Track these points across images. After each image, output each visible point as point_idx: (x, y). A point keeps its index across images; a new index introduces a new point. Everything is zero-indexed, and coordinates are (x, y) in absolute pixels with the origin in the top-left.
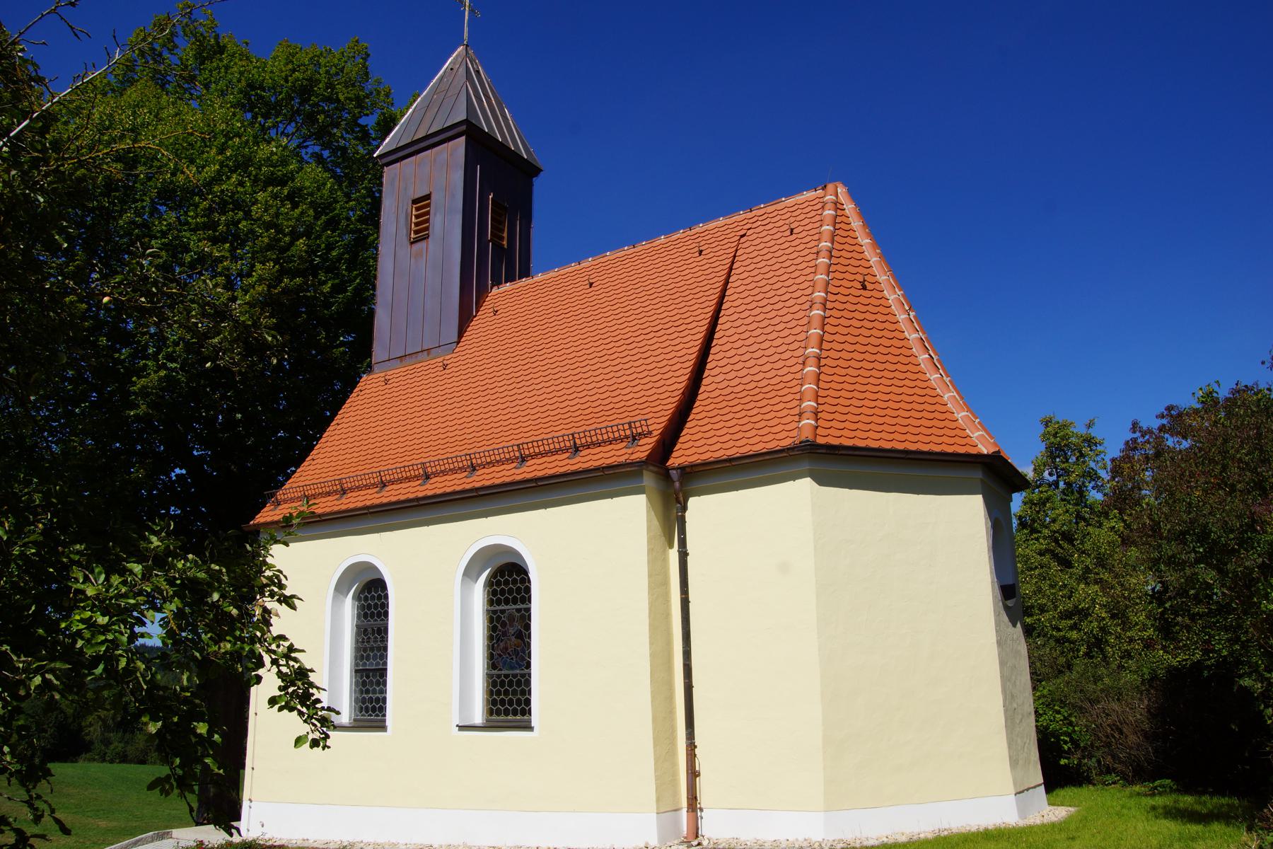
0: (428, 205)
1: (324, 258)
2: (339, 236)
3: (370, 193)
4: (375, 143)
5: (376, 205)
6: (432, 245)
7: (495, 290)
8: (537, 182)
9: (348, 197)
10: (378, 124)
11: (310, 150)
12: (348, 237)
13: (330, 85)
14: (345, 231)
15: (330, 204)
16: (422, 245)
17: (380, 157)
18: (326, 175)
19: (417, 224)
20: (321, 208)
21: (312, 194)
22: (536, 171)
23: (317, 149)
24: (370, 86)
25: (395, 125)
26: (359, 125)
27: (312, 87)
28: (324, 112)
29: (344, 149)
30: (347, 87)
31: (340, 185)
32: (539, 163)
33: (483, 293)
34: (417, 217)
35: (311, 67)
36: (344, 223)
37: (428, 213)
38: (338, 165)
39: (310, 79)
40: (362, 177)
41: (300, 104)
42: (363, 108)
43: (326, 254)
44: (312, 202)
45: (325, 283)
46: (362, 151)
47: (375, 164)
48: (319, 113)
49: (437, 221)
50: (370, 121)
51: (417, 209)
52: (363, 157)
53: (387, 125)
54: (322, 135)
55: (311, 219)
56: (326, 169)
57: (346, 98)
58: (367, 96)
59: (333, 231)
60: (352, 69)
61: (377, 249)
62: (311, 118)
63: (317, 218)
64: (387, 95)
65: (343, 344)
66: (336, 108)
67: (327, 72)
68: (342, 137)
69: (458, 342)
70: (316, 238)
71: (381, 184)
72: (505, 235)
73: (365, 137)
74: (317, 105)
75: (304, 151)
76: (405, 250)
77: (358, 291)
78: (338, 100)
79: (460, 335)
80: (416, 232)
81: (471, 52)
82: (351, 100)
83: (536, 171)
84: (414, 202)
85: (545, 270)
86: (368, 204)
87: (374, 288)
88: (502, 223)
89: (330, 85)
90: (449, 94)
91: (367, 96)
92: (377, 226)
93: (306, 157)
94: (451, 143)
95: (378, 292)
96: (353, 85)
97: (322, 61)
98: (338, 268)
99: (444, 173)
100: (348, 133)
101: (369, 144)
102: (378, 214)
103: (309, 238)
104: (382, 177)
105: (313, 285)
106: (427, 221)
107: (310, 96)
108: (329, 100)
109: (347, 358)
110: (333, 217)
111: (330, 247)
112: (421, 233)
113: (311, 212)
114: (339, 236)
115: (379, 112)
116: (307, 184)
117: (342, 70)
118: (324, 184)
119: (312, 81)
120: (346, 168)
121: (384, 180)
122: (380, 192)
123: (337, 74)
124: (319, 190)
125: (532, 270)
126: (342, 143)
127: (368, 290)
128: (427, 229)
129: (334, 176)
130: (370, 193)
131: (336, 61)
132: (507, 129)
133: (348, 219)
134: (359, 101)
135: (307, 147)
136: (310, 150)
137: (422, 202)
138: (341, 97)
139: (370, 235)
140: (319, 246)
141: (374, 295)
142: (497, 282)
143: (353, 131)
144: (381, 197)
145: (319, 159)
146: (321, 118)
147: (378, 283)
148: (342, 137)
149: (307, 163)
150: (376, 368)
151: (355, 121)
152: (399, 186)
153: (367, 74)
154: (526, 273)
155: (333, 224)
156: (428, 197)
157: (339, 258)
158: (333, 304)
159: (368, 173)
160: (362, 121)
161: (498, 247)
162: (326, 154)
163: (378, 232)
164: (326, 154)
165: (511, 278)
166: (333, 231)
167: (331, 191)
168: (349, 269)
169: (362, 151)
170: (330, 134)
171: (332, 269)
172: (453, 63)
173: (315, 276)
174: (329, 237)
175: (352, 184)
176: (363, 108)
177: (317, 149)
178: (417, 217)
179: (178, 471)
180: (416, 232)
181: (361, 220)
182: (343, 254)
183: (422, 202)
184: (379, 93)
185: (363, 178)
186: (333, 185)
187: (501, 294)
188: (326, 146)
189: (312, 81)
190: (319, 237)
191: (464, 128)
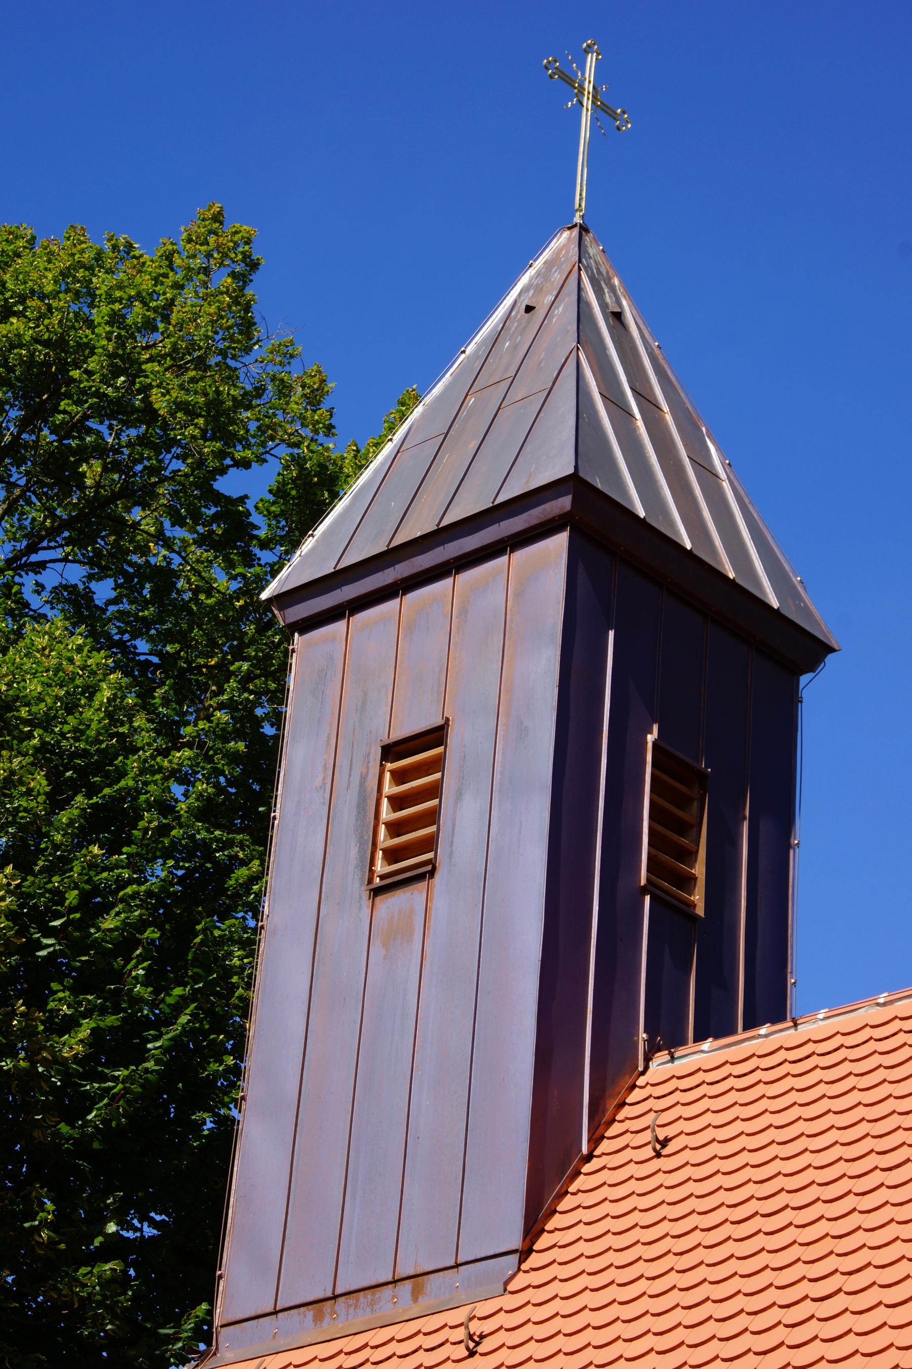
0: (437, 764)
1: (75, 939)
2: (130, 864)
3: (245, 722)
4: (267, 557)
5: (260, 763)
6: (446, 898)
7: (660, 1067)
8: (815, 691)
9: (169, 732)
10: (280, 492)
11: (50, 578)
12: (159, 870)
13: (125, 364)
14: (153, 850)
15: (108, 756)
16: (411, 898)
17: (285, 599)
18: (98, 658)
19: (395, 828)
20: (71, 772)
21: (46, 723)
22: (813, 651)
23: (75, 574)
24: (253, 368)
25: (335, 496)
26: (217, 498)
27: (64, 368)
28: (100, 450)
29: (164, 578)
30: (179, 370)
31: (145, 695)
32: (821, 616)
33: (615, 1073)
34: (398, 802)
35: (65, 298)
36: (150, 820)
37: (434, 791)
38: (140, 628)
39: (59, 344)
40: (218, 666)
41: (24, 424)
42: (230, 439)
43: (83, 925)
44: (44, 747)
45: (69, 1025)
46: (223, 582)
47: (264, 627)
48: (84, 454)
49: (462, 820)
50: (252, 485)
51: (400, 777)
52: (227, 601)
53: (309, 496)
54: (94, 527)
55: (38, 805)
56: (99, 641)
57: (180, 406)
58: (244, 403)
59: (113, 848)
60: (196, 310)
61: (256, 910)
62: (59, 470)
63: (57, 800)
64: (314, 399)
65: (115, 1248)
66: (142, 441)
67: (115, 319)
68: (160, 537)
69: (525, 1253)
70: (49, 871)
71: (279, 695)
72: (699, 870)
73: (232, 533)
74: (79, 427)
75: (29, 580)
76: (350, 912)
77: (184, 1058)
78: (149, 414)
79: (535, 1221)
80: (392, 855)
81: (594, 250)
82: (191, 411)
83: (813, 651)
84: (390, 751)
85: (841, 999)
86: (234, 758)
87: (240, 1052)
88: (689, 828)
89: (125, 364)
90: (519, 392)
91: (244, 403)
92: (260, 831)
93: (36, 602)
94: (521, 556)
95: (253, 1063)
96: (201, 364)
97: (101, 282)
98: (119, 976)
99: (495, 658)
100: (178, 521)
101: (249, 559)
102: (267, 796)
103: (24, 868)
104: (284, 668)
105: (28, 1032)
106: (432, 817)
107: (57, 396)
108: (117, 410)
109: (125, 1300)
110: (117, 800)
111: (94, 904)
112: (407, 858)
113: (40, 781)
114: (130, 864)
115: (283, 452)
116: (34, 687)
117: (165, 312)
118: (91, 691)
119: (65, 349)
120: (168, 637)
121: (292, 682)
122: (278, 719)
123: (149, 326)
124: (71, 708)
125: (795, 999)
126: (159, 555)
127: (218, 1053)
128: (430, 843)
129: (127, 662)
130: (245, 722)
131: (146, 283)
132: (718, 515)
133: (166, 807)
134: (220, 420)
135: (40, 566)
136: (50, 578)
137: (416, 753)
138: (160, 403)
139: (236, 862)
140: (58, 896)
141: (237, 1072)
142: (666, 1037)
143: (196, 516)
144: (277, 739)
145: (78, 605)
146: (92, 470)
147: (256, 1029)
148: (160, 537)
149: (39, 618)
150: (225, 1338)
151: (204, 479)
152: (339, 700)
153: (247, 326)
154: (770, 1006)
155: (111, 823)
156: (436, 736)
157: (126, 943)
158: (89, 1101)
159: (238, 655)
160: (229, 484)
161: (672, 912)
162: (104, 590)
163: (263, 857)
164: (104, 590)
165: (714, 1025)
166: (113, 848)
167: (114, 712)
168: (154, 979)
169: (223, 582)
170: (121, 527)
171: (98, 978)
172: (535, 287)
173: (37, 1000)
174: (92, 866)
175: (187, 690)
176: (230, 439)
177: (75, 574)
178: (398, 802)
179: (209, 1125)
180: (392, 855)
181: (208, 811)
182: (142, 925)
183: (416, 753)
184: (284, 390)
185: (222, 673)
186: (120, 692)
187: (683, 1079)
188: (100, 567)
189: (65, 349)
190: (61, 865)
191: (565, 503)
